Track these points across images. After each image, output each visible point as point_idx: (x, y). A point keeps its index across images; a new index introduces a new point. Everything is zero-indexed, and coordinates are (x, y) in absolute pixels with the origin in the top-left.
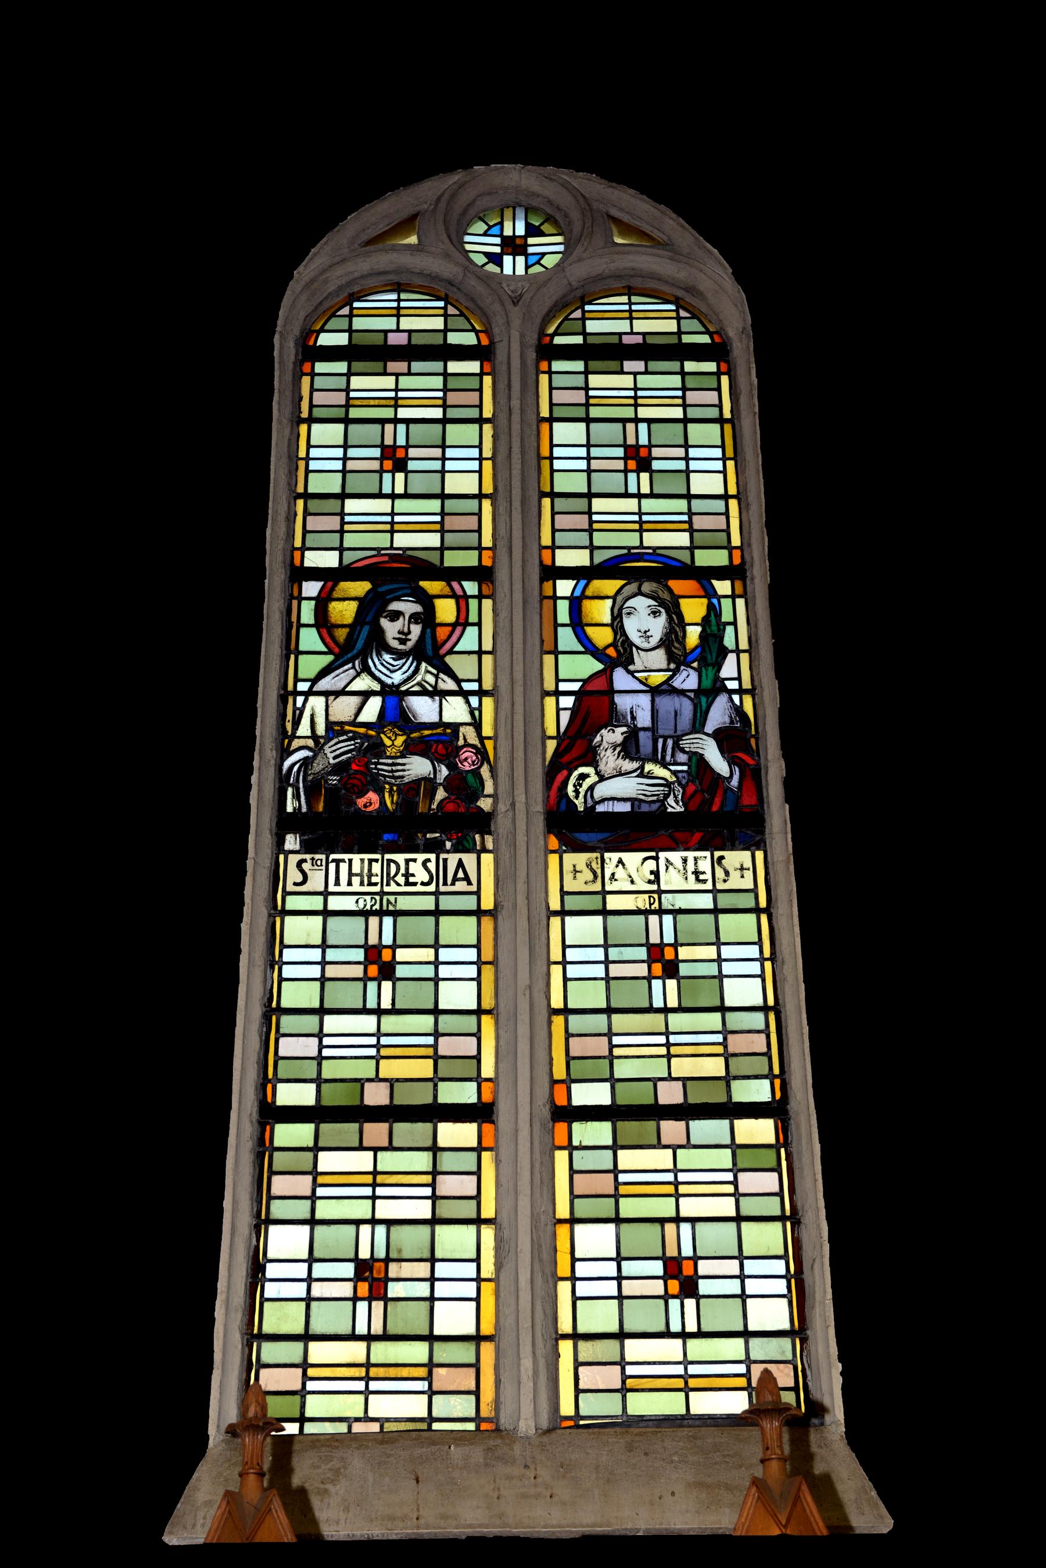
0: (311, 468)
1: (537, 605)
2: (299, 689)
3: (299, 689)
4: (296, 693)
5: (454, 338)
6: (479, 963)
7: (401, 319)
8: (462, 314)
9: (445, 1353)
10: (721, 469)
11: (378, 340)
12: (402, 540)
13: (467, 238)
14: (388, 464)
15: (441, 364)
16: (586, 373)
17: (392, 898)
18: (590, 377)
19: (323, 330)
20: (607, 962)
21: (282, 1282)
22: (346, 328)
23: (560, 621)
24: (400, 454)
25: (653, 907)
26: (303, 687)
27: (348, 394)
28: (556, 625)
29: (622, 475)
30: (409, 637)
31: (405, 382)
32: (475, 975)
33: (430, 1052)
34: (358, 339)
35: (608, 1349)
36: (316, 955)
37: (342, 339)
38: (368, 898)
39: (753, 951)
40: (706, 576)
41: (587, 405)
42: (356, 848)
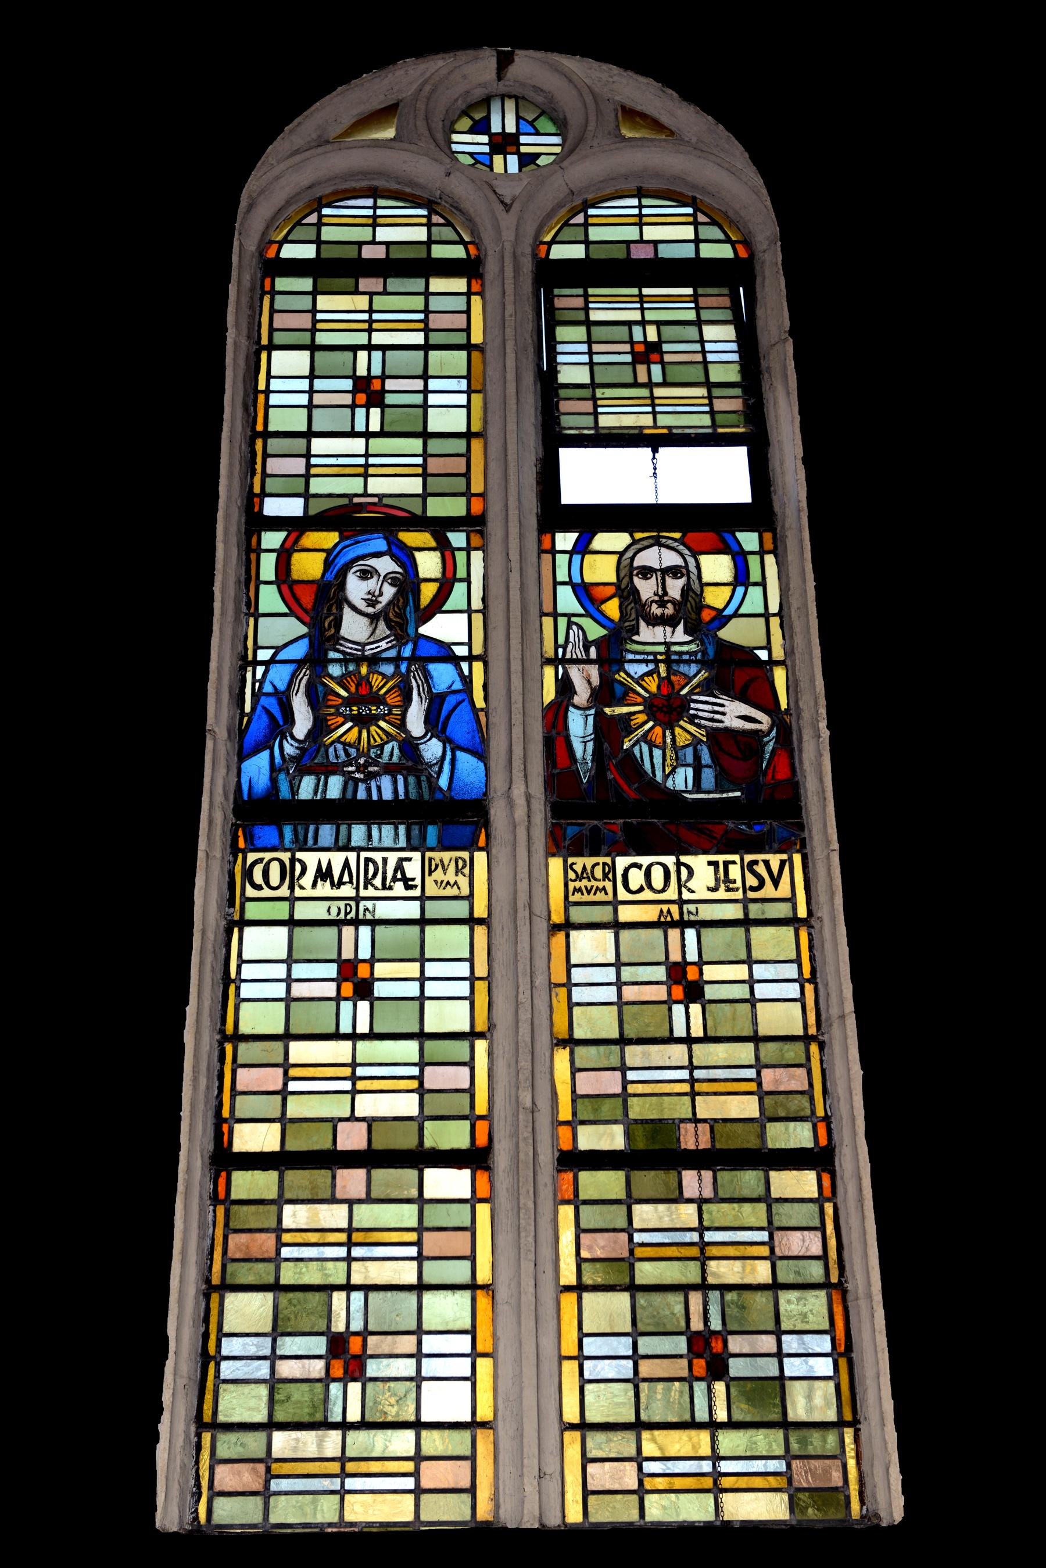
0: (271, 403)
1: (535, 559)
2: (259, 658)
3: (259, 658)
4: (255, 663)
5: (439, 252)
6: (472, 979)
7: (378, 229)
8: (448, 224)
9: (434, 1442)
10: (465, 403)
11: (351, 253)
12: (377, 486)
13: (455, 137)
14: (362, 398)
15: (423, 281)
16: (314, 293)
17: (369, 904)
18: (319, 298)
19: (286, 240)
20: (289, 980)
21: (242, 1356)
22: (314, 238)
23: (559, 579)
24: (376, 385)
25: (349, 917)
26: (264, 655)
27: (314, 316)
28: (259, 582)
29: (348, 411)
30: (380, 599)
31: (379, 302)
32: (467, 994)
33: (415, 1084)
34: (327, 253)
35: (623, 1444)
36: (610, 974)
37: (308, 252)
38: (342, 904)
39: (791, 971)
40: (440, 527)
41: (313, 331)
42: (776, 846)
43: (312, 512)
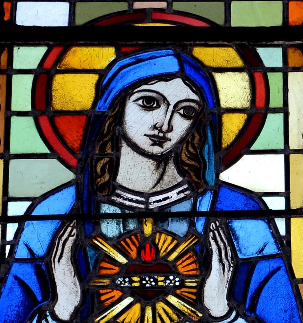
2: (10, 213)
3: (10, 213)
23: (15, 107)
26: (16, 209)
30: (169, 135)
40: (248, 41)
43: (80, 21)
